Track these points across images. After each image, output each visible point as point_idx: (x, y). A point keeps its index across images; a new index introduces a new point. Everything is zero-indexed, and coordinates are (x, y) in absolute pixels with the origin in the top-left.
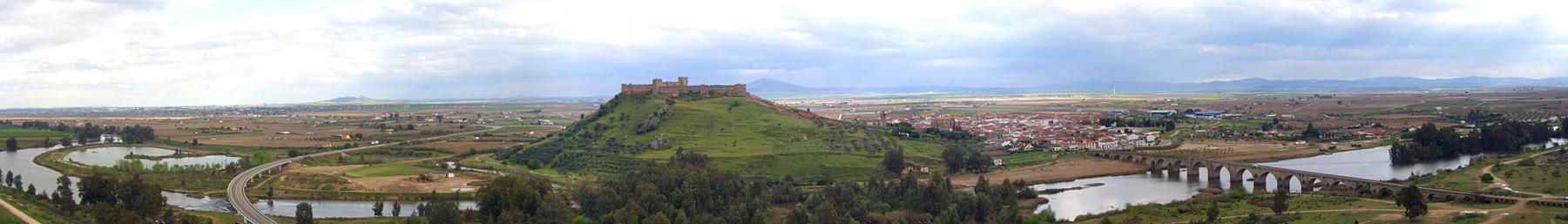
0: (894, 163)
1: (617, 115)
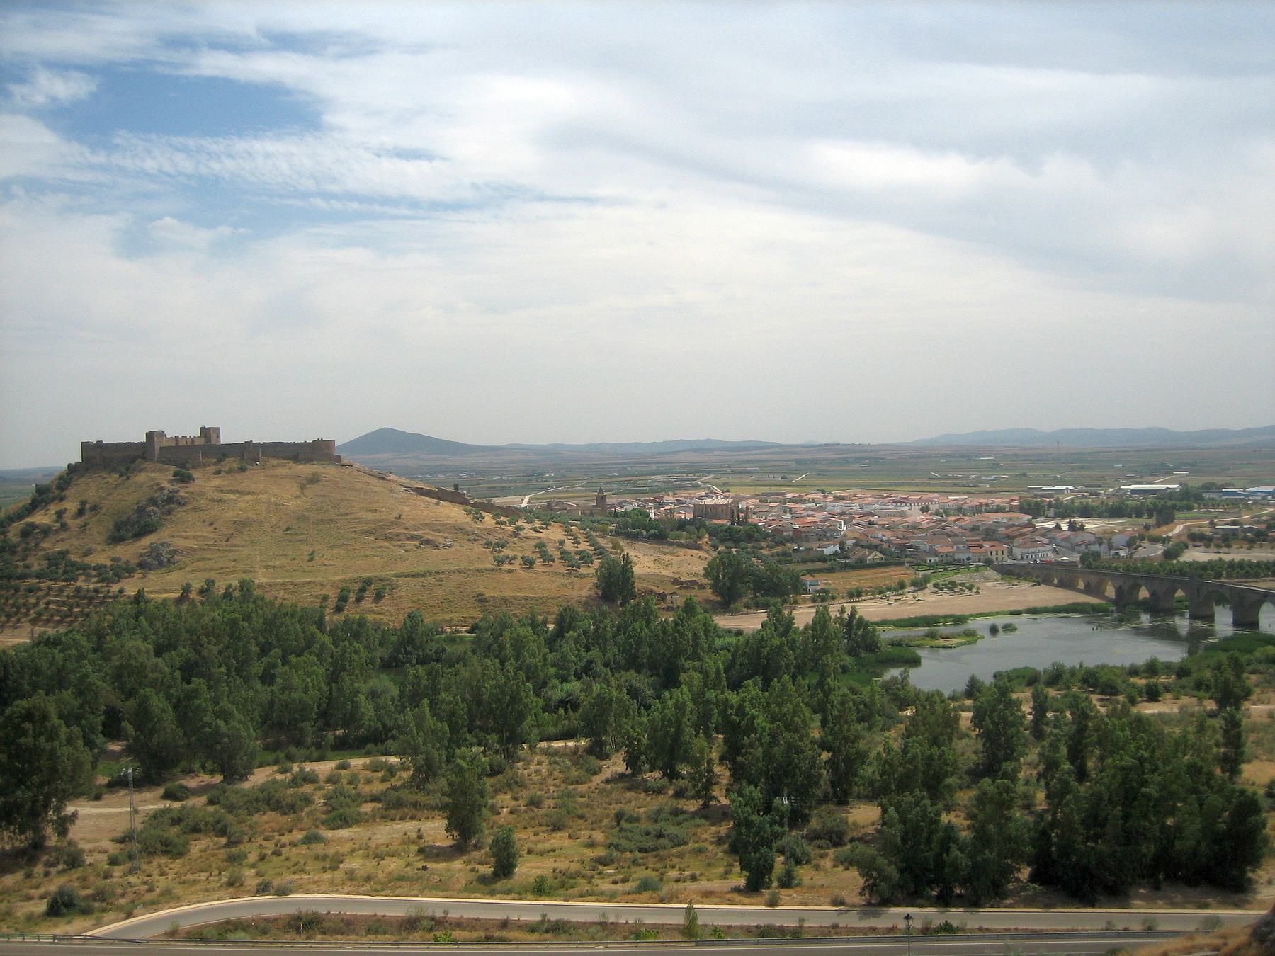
0: (616, 584)
1: (71, 506)
